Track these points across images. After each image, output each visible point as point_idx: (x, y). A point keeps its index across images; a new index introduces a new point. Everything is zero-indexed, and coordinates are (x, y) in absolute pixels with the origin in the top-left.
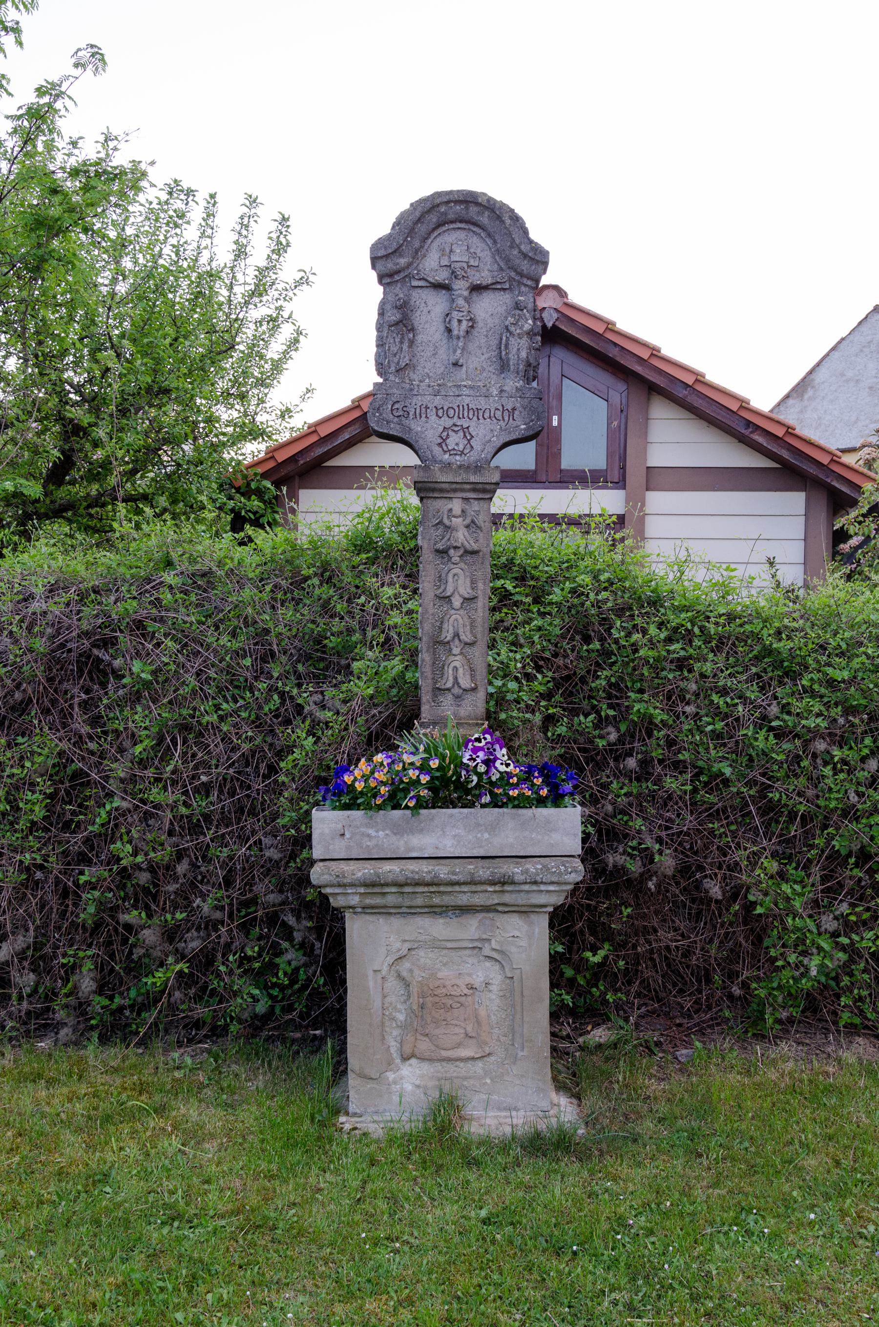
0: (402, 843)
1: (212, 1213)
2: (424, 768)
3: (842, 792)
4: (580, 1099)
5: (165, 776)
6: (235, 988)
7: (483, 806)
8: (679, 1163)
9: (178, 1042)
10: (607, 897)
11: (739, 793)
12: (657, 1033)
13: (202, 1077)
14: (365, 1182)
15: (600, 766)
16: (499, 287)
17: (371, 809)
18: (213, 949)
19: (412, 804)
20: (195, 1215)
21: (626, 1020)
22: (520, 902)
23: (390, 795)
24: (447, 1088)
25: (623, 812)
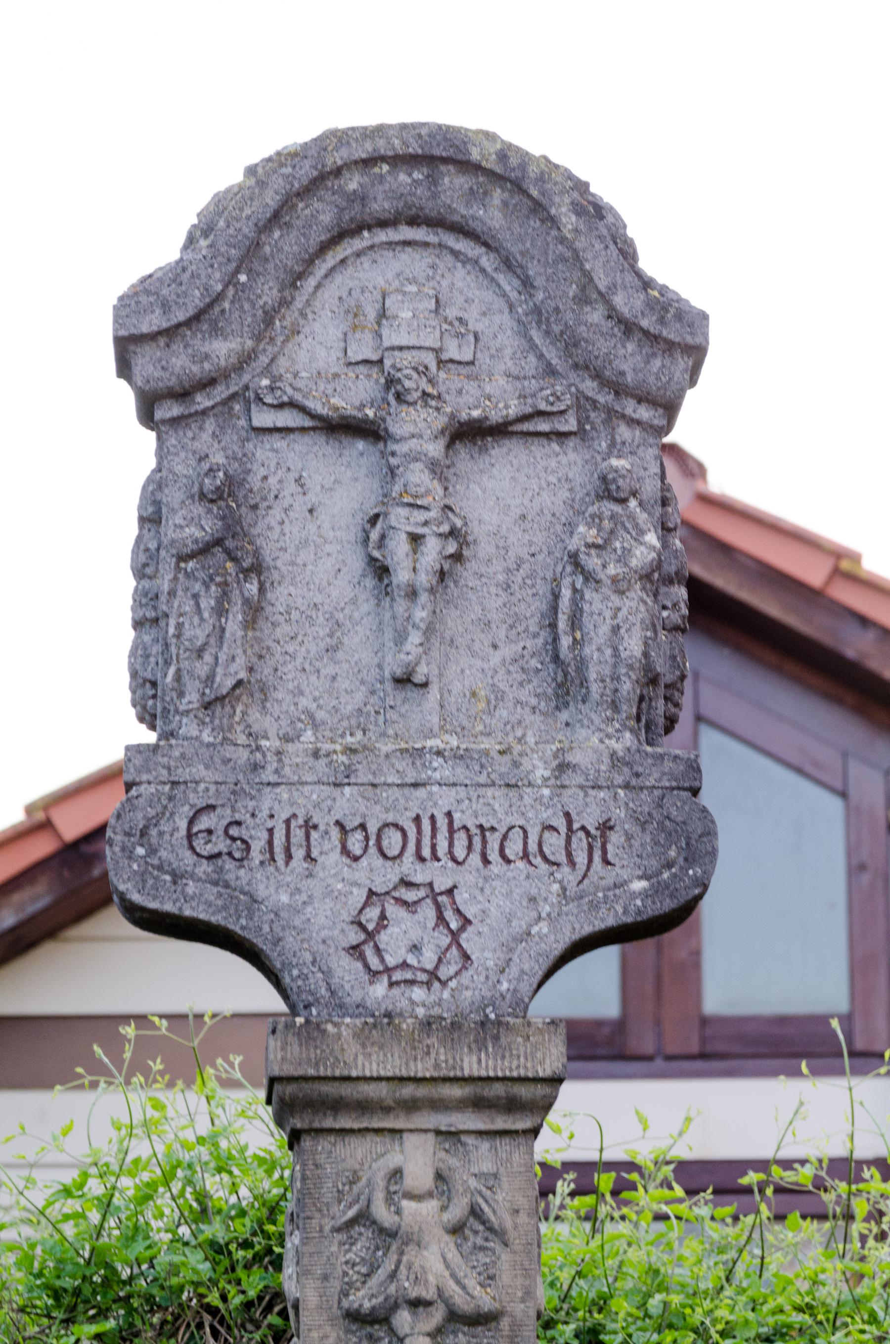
16: (543, 426)
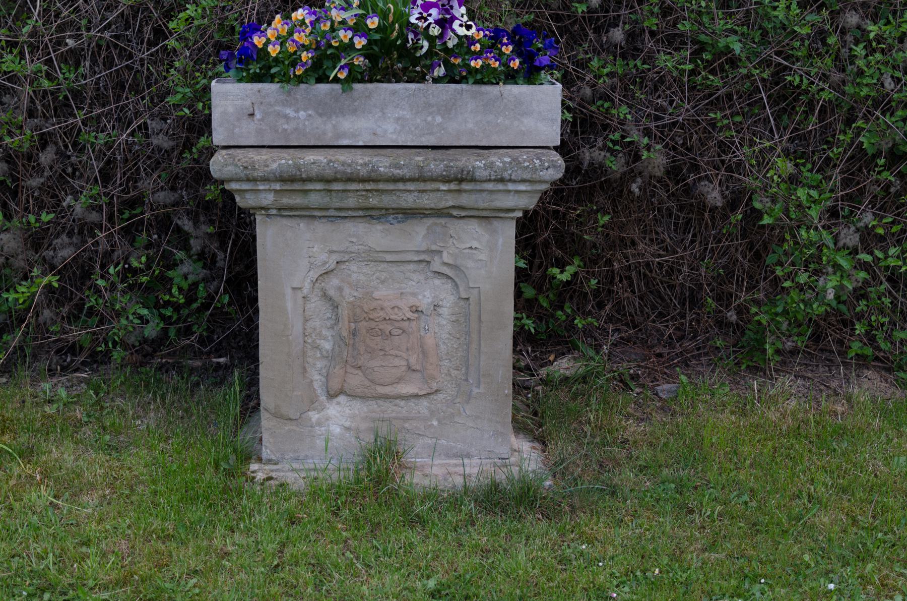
0: (329, 127)
1: (91, 583)
2: (359, 28)
3: (877, 75)
4: (544, 443)
5: (21, 39)
6: (118, 307)
7: (436, 81)
8: (667, 522)
9: (49, 370)
10: (579, 202)
11: (749, 76)
12: (632, 365)
13: (79, 413)
14: (283, 545)
15: (575, 40)
17: (288, 81)
18: (90, 259)
19: (342, 75)
20: (71, 585)
21: (597, 349)
22: (481, 205)
23: (314, 63)
24: (383, 430)
25: (606, 98)
